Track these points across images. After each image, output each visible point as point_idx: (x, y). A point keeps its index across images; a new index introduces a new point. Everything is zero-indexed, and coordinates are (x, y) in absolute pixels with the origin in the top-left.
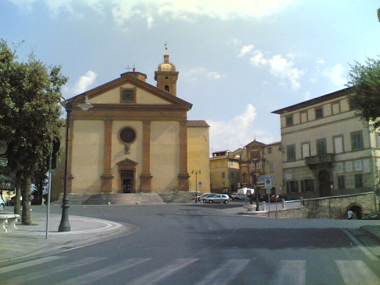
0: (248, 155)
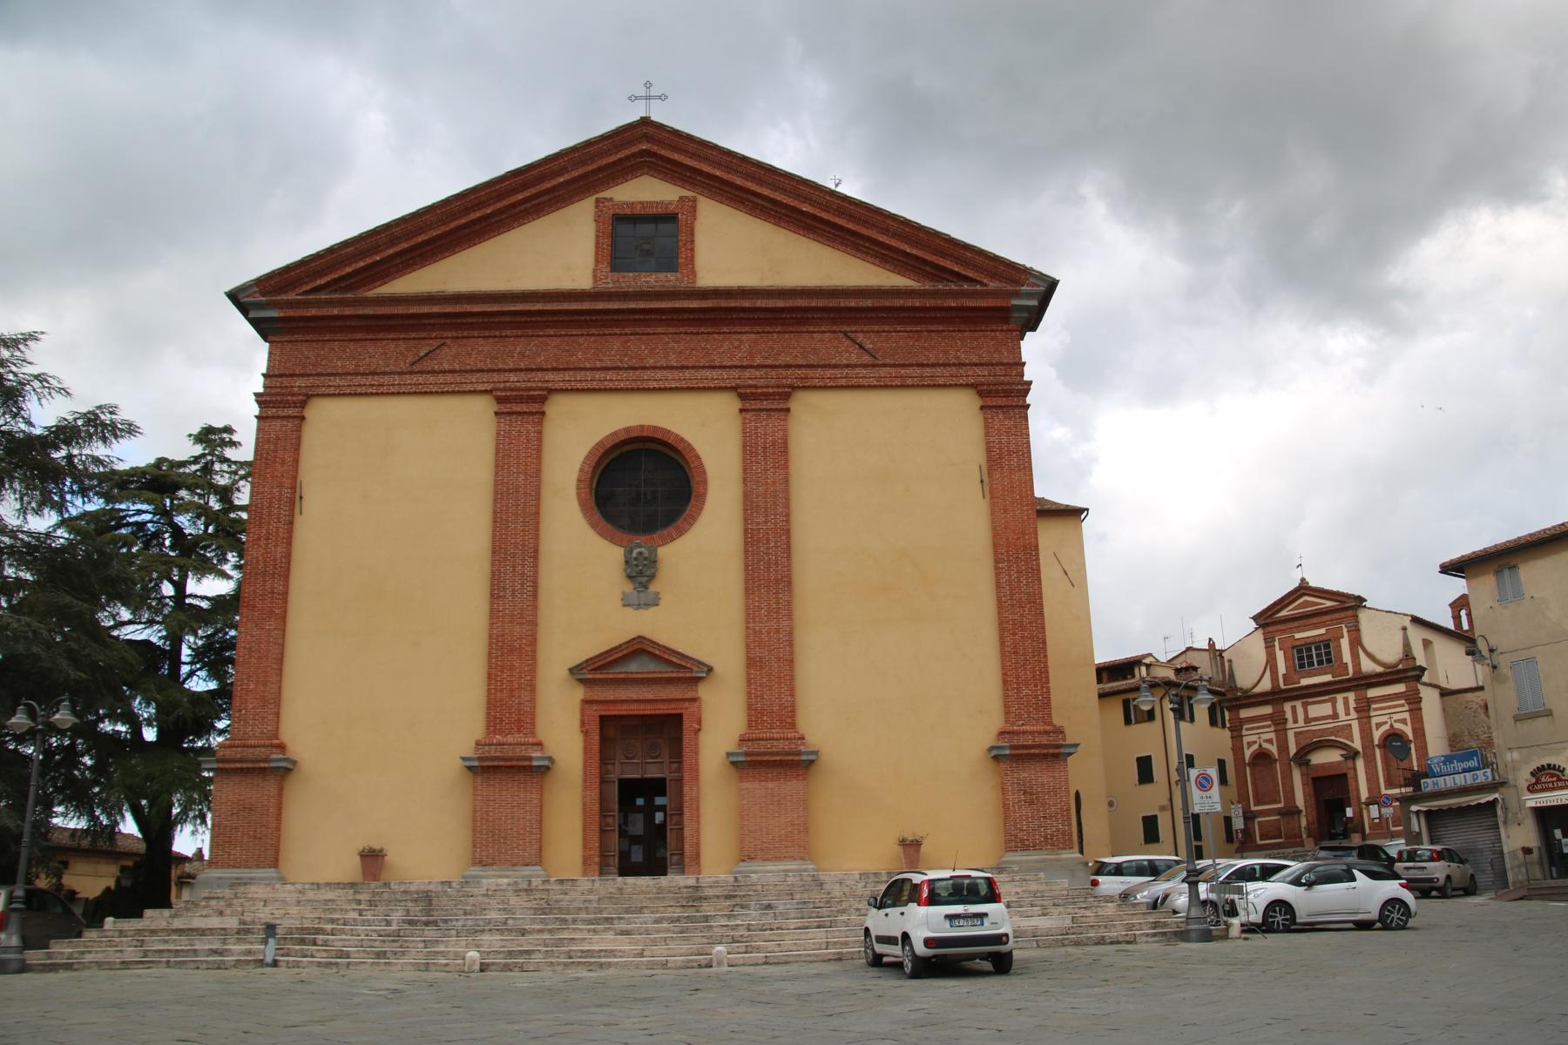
0: (1271, 661)
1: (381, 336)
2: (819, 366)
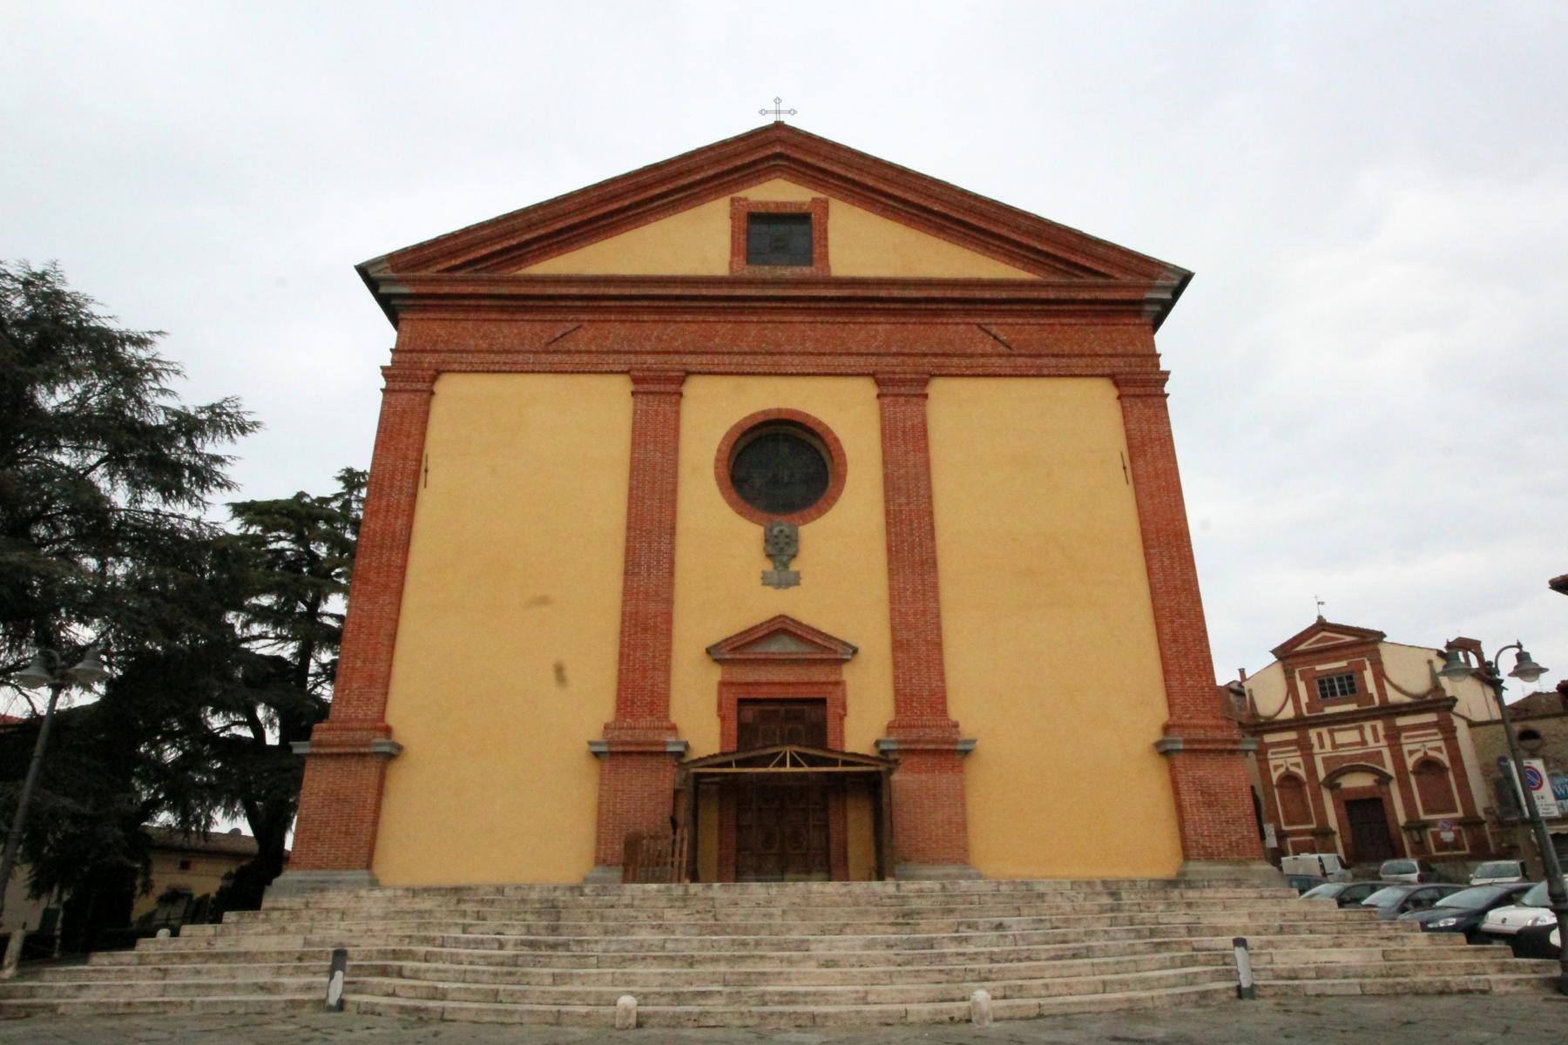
0: (1292, 690)
2: (955, 355)
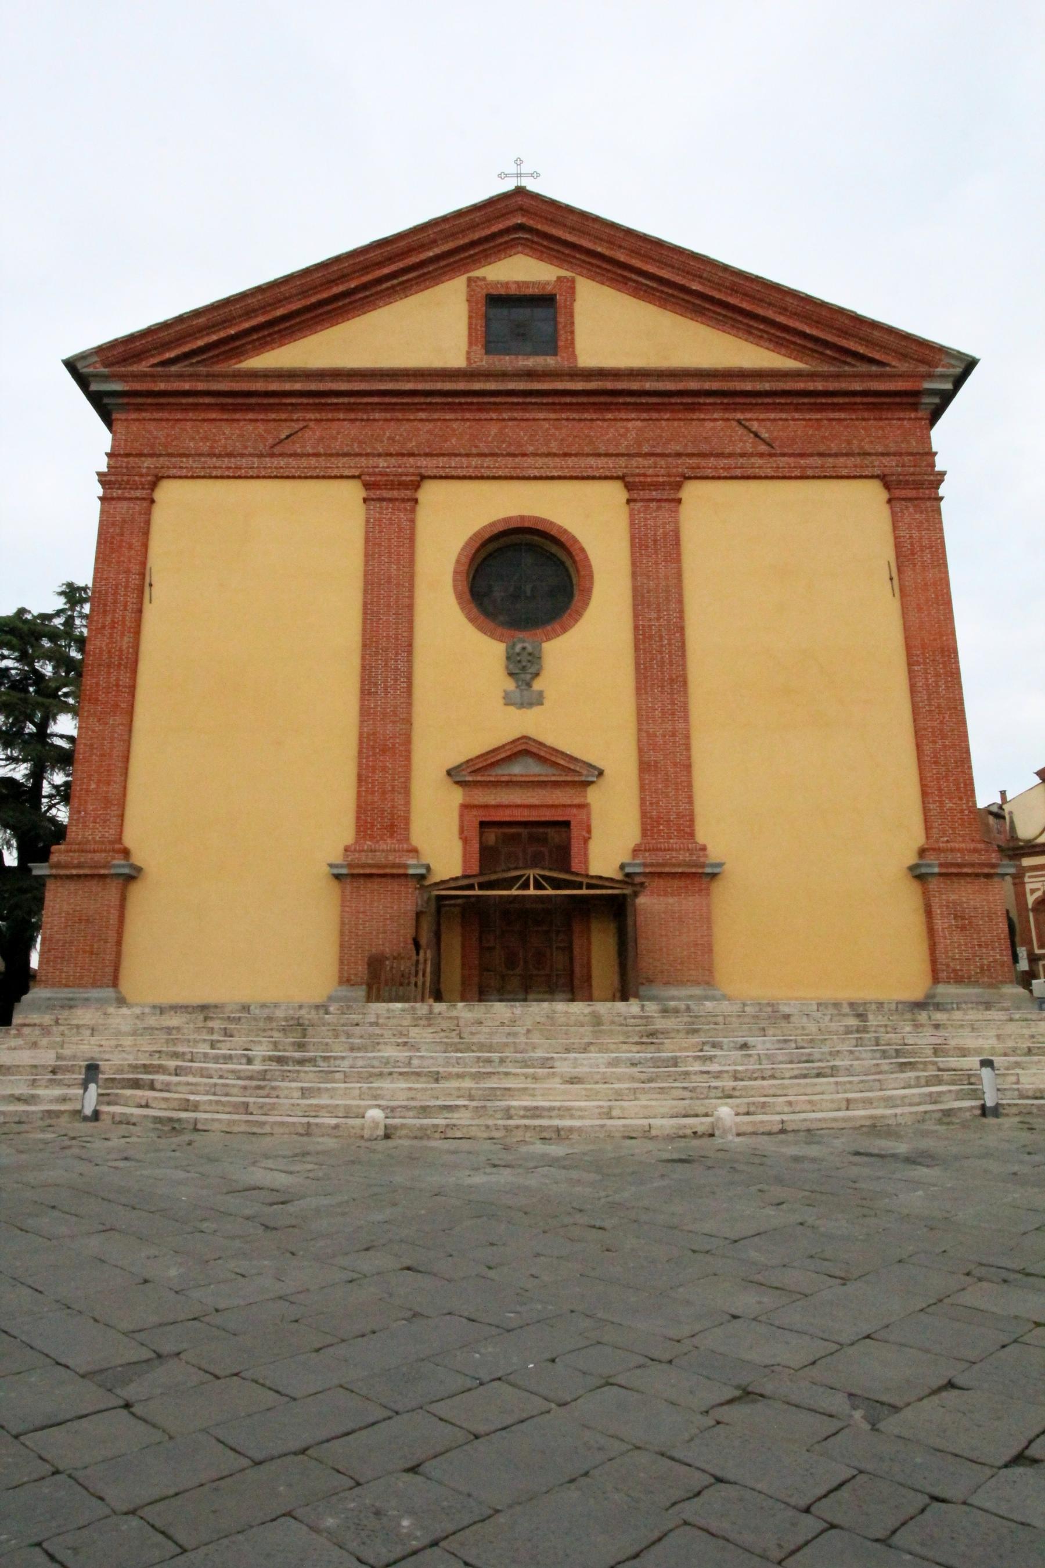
1: (237, 416)
2: (711, 455)
